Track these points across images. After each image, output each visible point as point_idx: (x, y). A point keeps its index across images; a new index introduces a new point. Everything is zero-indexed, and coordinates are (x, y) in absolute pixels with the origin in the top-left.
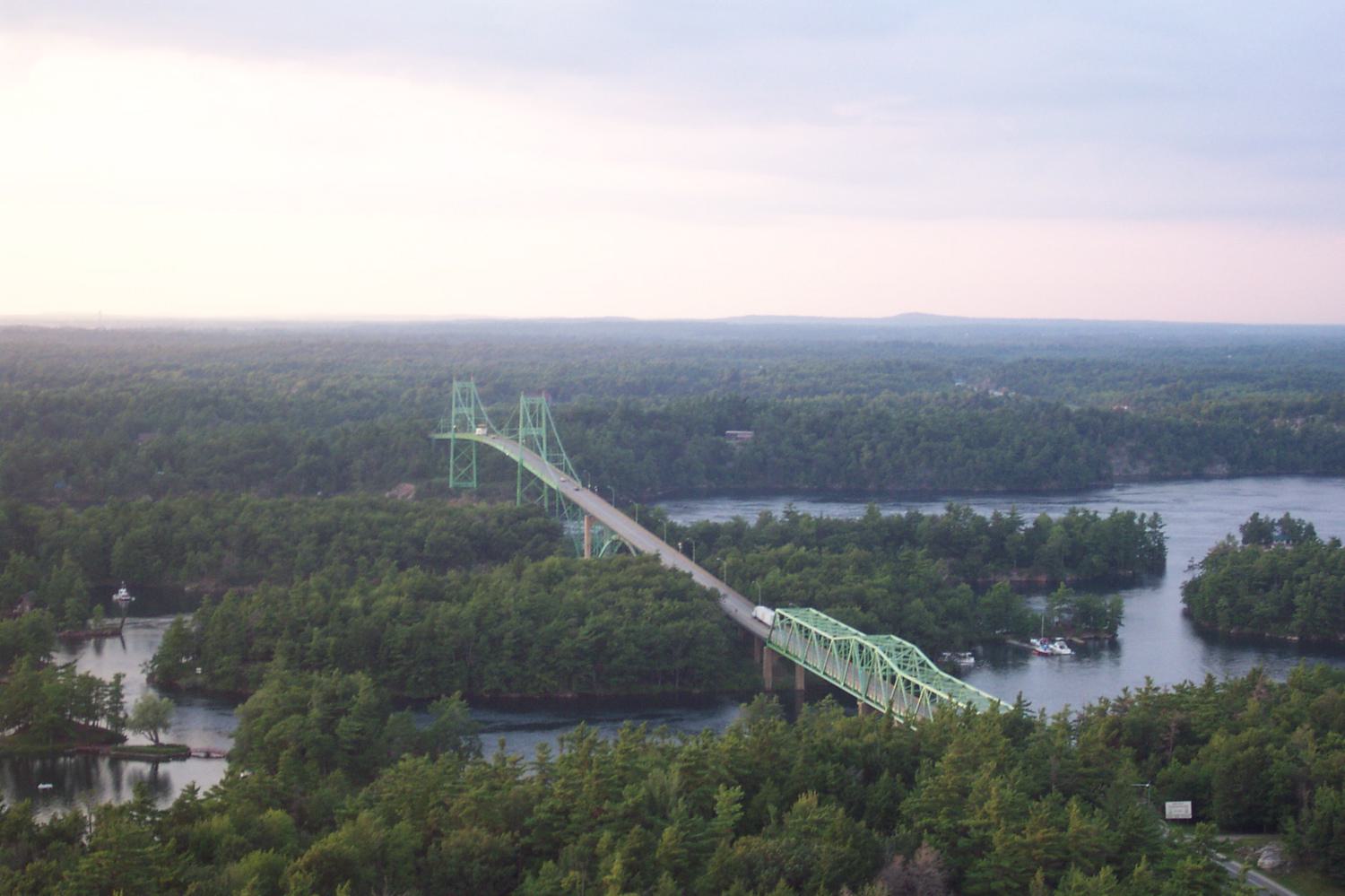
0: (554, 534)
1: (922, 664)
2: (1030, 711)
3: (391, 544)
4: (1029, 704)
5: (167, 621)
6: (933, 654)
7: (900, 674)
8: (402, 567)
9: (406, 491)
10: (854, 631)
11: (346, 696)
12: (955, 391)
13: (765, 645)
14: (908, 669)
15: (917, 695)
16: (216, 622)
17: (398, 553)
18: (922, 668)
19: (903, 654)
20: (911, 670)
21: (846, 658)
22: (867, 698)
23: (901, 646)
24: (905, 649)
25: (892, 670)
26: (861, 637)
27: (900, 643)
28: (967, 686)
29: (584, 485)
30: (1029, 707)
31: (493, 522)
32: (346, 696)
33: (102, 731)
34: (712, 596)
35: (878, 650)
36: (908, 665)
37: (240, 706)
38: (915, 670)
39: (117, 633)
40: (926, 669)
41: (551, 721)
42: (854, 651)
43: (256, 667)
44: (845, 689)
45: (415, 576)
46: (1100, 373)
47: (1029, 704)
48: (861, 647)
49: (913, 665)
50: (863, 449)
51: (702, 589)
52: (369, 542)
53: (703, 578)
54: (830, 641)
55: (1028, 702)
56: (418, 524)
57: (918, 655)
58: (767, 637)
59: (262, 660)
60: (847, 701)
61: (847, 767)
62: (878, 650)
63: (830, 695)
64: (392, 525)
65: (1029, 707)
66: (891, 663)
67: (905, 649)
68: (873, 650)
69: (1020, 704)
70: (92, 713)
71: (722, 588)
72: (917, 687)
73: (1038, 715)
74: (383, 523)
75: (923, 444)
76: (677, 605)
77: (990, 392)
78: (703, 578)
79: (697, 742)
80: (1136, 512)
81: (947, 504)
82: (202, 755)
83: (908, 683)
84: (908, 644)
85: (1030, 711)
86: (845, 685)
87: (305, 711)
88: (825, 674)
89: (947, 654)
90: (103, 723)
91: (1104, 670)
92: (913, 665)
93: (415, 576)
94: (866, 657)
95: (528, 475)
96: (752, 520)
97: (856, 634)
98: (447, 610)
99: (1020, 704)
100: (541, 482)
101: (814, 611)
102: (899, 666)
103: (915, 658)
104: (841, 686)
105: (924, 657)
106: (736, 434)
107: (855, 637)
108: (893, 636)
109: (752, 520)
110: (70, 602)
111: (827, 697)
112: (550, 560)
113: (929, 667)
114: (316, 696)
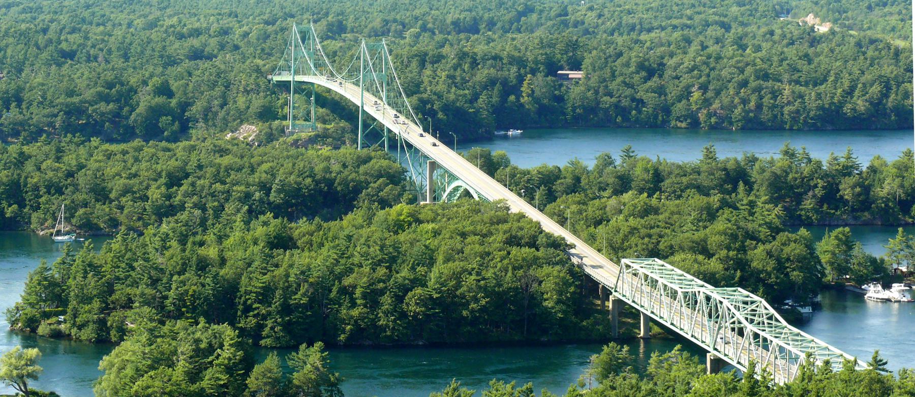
0: (396, 178)
1: (770, 318)
2: (887, 371)
4: (886, 363)
8: (253, 214)
9: (249, 131)
10: (701, 283)
14: (755, 322)
17: (247, 197)
20: (759, 323)
21: (695, 310)
23: (749, 299)
24: (752, 302)
25: (740, 323)
26: (709, 289)
28: (816, 340)
30: (885, 367)
31: (336, 167)
32: (211, 349)
34: (557, 244)
36: (756, 318)
37: (104, 358)
38: (763, 323)
40: (773, 322)
42: (701, 298)
44: (693, 340)
47: (886, 363)
49: (761, 319)
50: (693, 89)
51: (549, 236)
53: (550, 226)
54: (657, 281)
55: (884, 361)
57: (766, 308)
58: (613, 286)
59: (123, 307)
60: (696, 351)
65: (885, 367)
66: (740, 316)
67: (752, 302)
68: (721, 303)
71: (570, 238)
72: (765, 340)
73: (898, 378)
74: (228, 169)
75: (753, 84)
78: (550, 226)
83: (756, 336)
85: (887, 371)
86: (692, 336)
87: (171, 365)
89: (790, 302)
91: (887, 292)
92: (761, 319)
96: (590, 164)
101: (660, 262)
102: (747, 319)
104: (689, 337)
105: (772, 311)
106: (568, 74)
108: (739, 289)
109: (590, 164)
111: (676, 348)
112: (398, 207)
113: (777, 320)
114: (185, 348)
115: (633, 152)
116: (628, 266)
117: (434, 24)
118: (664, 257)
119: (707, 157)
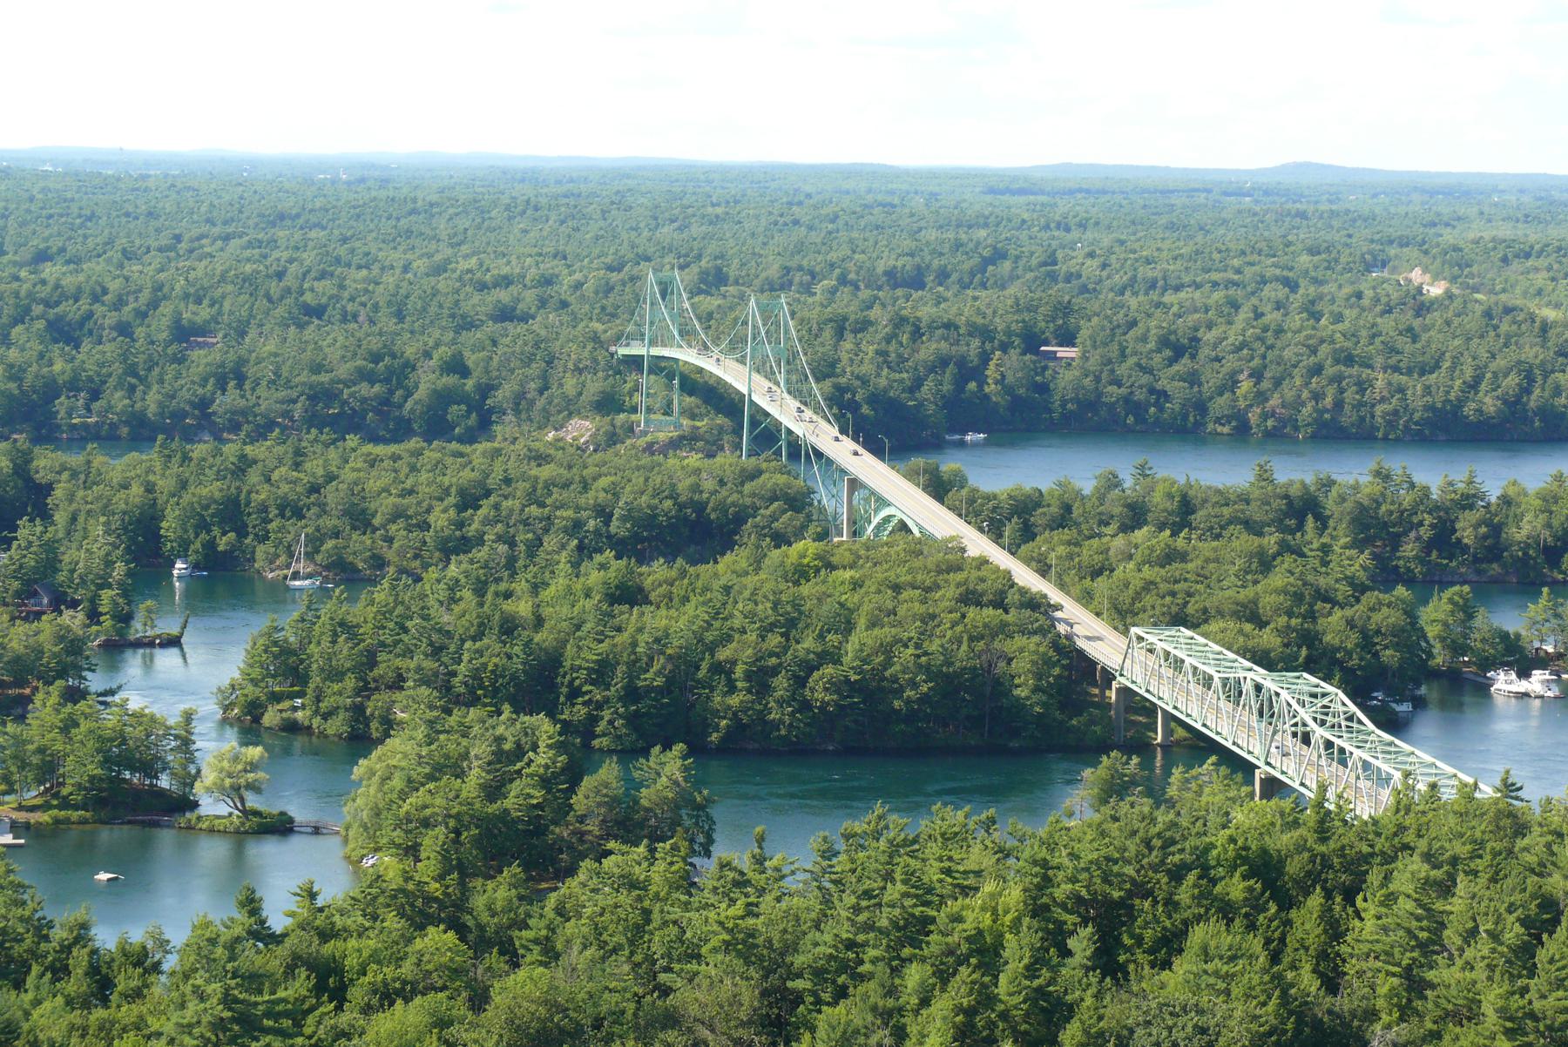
0: (798, 502)
1: (1350, 718)
2: (1522, 800)
3: (565, 514)
6: (1358, 693)
7: (1319, 733)
10: (1248, 664)
12: (1374, 288)
13: (1115, 678)
15: (1343, 762)
16: (323, 633)
18: (1350, 724)
19: (1320, 702)
20: (1333, 726)
22: (1268, 764)
24: (1324, 695)
25: (1305, 725)
26: (1259, 674)
29: (843, 431)
30: (1520, 793)
33: (162, 793)
34: (1036, 604)
35: (1284, 695)
36: (1329, 719)
37: (361, 762)
38: (1340, 726)
39: (174, 642)
40: (1355, 725)
41: (1006, 198)
42: (1248, 687)
45: (605, 570)
47: (1521, 788)
49: (1336, 720)
51: (1023, 591)
52: (534, 510)
55: (1518, 785)
56: (604, 482)
57: (1344, 704)
59: (390, 687)
60: (1240, 767)
62: (1284, 695)
63: (1213, 758)
66: (1305, 715)
67: (1324, 695)
69: (1509, 788)
70: (149, 767)
71: (1055, 595)
72: (1342, 751)
73: (1538, 811)
74: (549, 485)
75: (1330, 371)
77: (1425, 287)
78: (1026, 578)
79: (1091, 1018)
80: (1430, 485)
85: (1522, 800)
86: (1234, 743)
87: (460, 774)
88: (1204, 725)
89: (1380, 695)
90: (164, 782)
92: (1336, 720)
93: (605, 570)
94: (1267, 710)
95: (759, 414)
96: (1087, 485)
98: (655, 620)
99: (1509, 788)
102: (1315, 719)
104: (1229, 745)
105: (1353, 708)
106: (1055, 352)
109: (1087, 485)
110: (106, 595)
111: (1209, 761)
112: (799, 546)
114: (481, 750)
115: (1150, 469)
116: (1140, 639)
117: (858, 273)
118: (1193, 626)
119: (1260, 478)
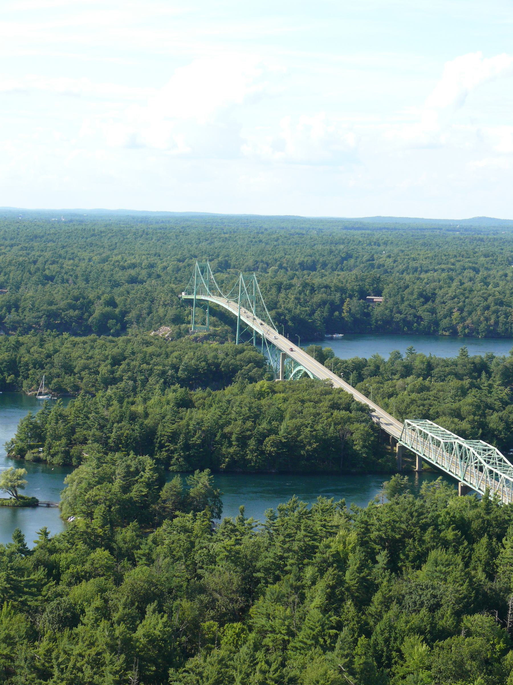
1: (500, 460)
5: (26, 413)
7: (487, 467)
11: (137, 472)
13: (398, 442)
19: (487, 453)
20: (493, 464)
24: (489, 450)
25: (481, 463)
26: (461, 441)
27: (486, 446)
31: (221, 356)
32: (137, 472)
35: (472, 450)
36: (491, 460)
42: (456, 446)
43: (78, 447)
46: (464, 302)
48: (460, 447)
51: (358, 403)
52: (145, 366)
53: (359, 397)
57: (498, 454)
60: (452, 481)
61: (351, 412)
62: (472, 450)
64: (159, 355)
66: (480, 458)
67: (489, 450)
71: (372, 405)
72: (497, 474)
74: (152, 355)
76: (343, 413)
78: (359, 397)
81: (409, 347)
82: (45, 505)
83: (491, 472)
84: (491, 447)
86: (450, 471)
88: (437, 463)
94: (464, 456)
95: (244, 325)
96: (387, 357)
97: (457, 439)
98: (197, 414)
100: (252, 329)
102: (485, 461)
103: (497, 456)
105: (501, 456)
107: (457, 441)
108: (481, 441)
113: (505, 462)
